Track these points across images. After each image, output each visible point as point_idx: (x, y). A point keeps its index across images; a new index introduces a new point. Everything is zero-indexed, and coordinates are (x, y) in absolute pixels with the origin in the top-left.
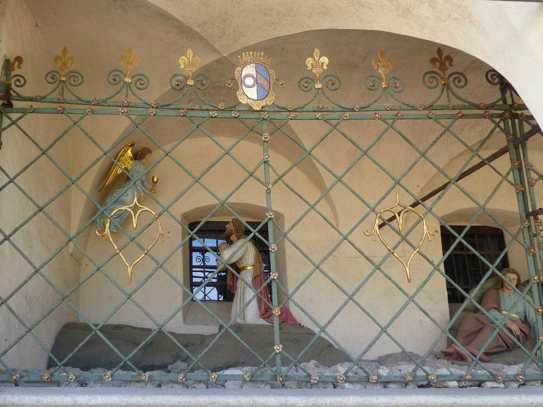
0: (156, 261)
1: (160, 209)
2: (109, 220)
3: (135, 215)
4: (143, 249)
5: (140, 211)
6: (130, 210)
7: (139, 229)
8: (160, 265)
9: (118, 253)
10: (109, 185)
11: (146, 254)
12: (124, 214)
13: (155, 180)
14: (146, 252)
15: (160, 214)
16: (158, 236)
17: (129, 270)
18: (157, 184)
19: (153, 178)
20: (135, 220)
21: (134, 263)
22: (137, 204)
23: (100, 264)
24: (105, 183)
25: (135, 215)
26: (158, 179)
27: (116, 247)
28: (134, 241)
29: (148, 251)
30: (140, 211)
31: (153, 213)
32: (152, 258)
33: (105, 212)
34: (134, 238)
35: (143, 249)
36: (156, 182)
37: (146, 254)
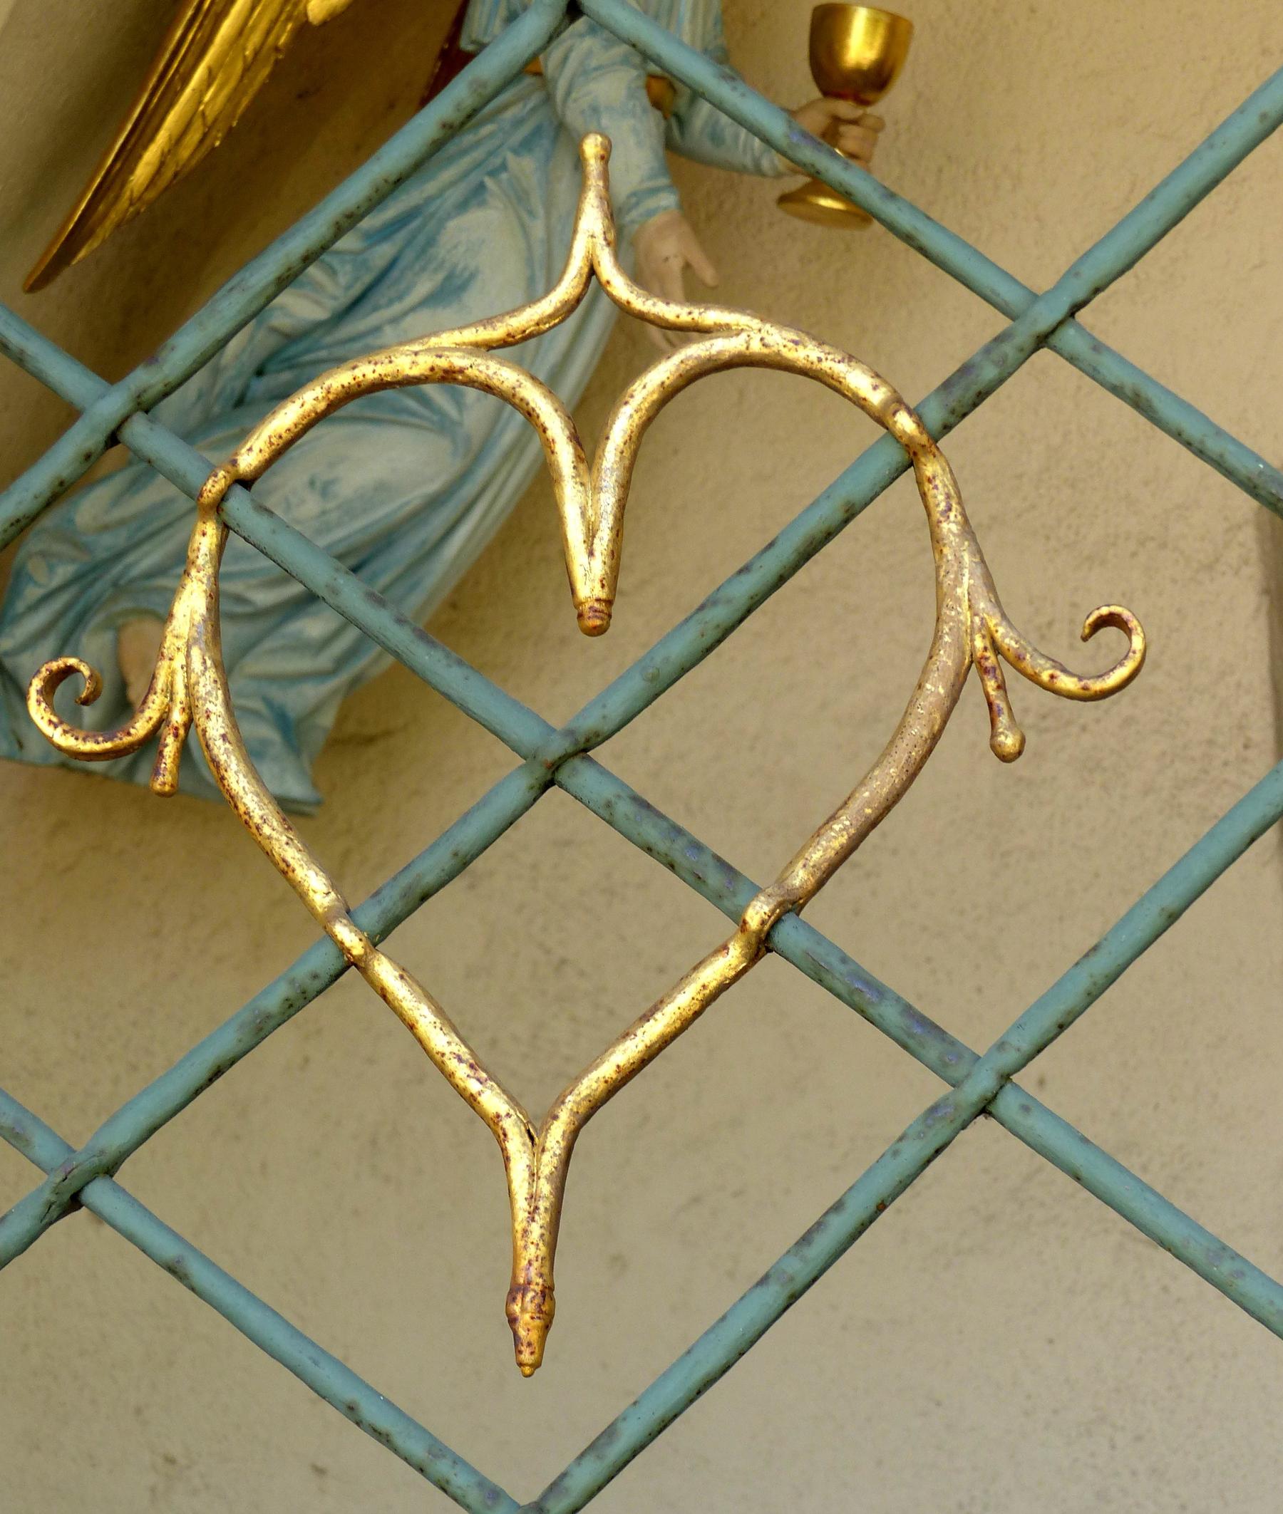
0: (918, 1034)
1: (958, 329)
2: (206, 539)
3: (587, 443)
4: (720, 882)
5: (662, 373)
6: (506, 376)
7: (645, 633)
8: (982, 1083)
9: (349, 963)
10: (178, 185)
11: (762, 945)
12: (405, 550)
13: (860, 45)
14: (757, 913)
15: (966, 395)
16: (936, 688)
17: (526, 1172)
18: (894, 104)
19: (826, 28)
20: (585, 509)
21: (591, 1083)
22: (621, 287)
23: (89, 1135)
24: (130, 155)
25: (587, 443)
26: (896, 33)
27: (316, 886)
28: (582, 776)
29: (792, 906)
30: (662, 373)
31: (858, 380)
32: (861, 995)
33: (140, 433)
34: (583, 748)
35: (720, 882)
36: (877, 79)
37: (762, 945)
